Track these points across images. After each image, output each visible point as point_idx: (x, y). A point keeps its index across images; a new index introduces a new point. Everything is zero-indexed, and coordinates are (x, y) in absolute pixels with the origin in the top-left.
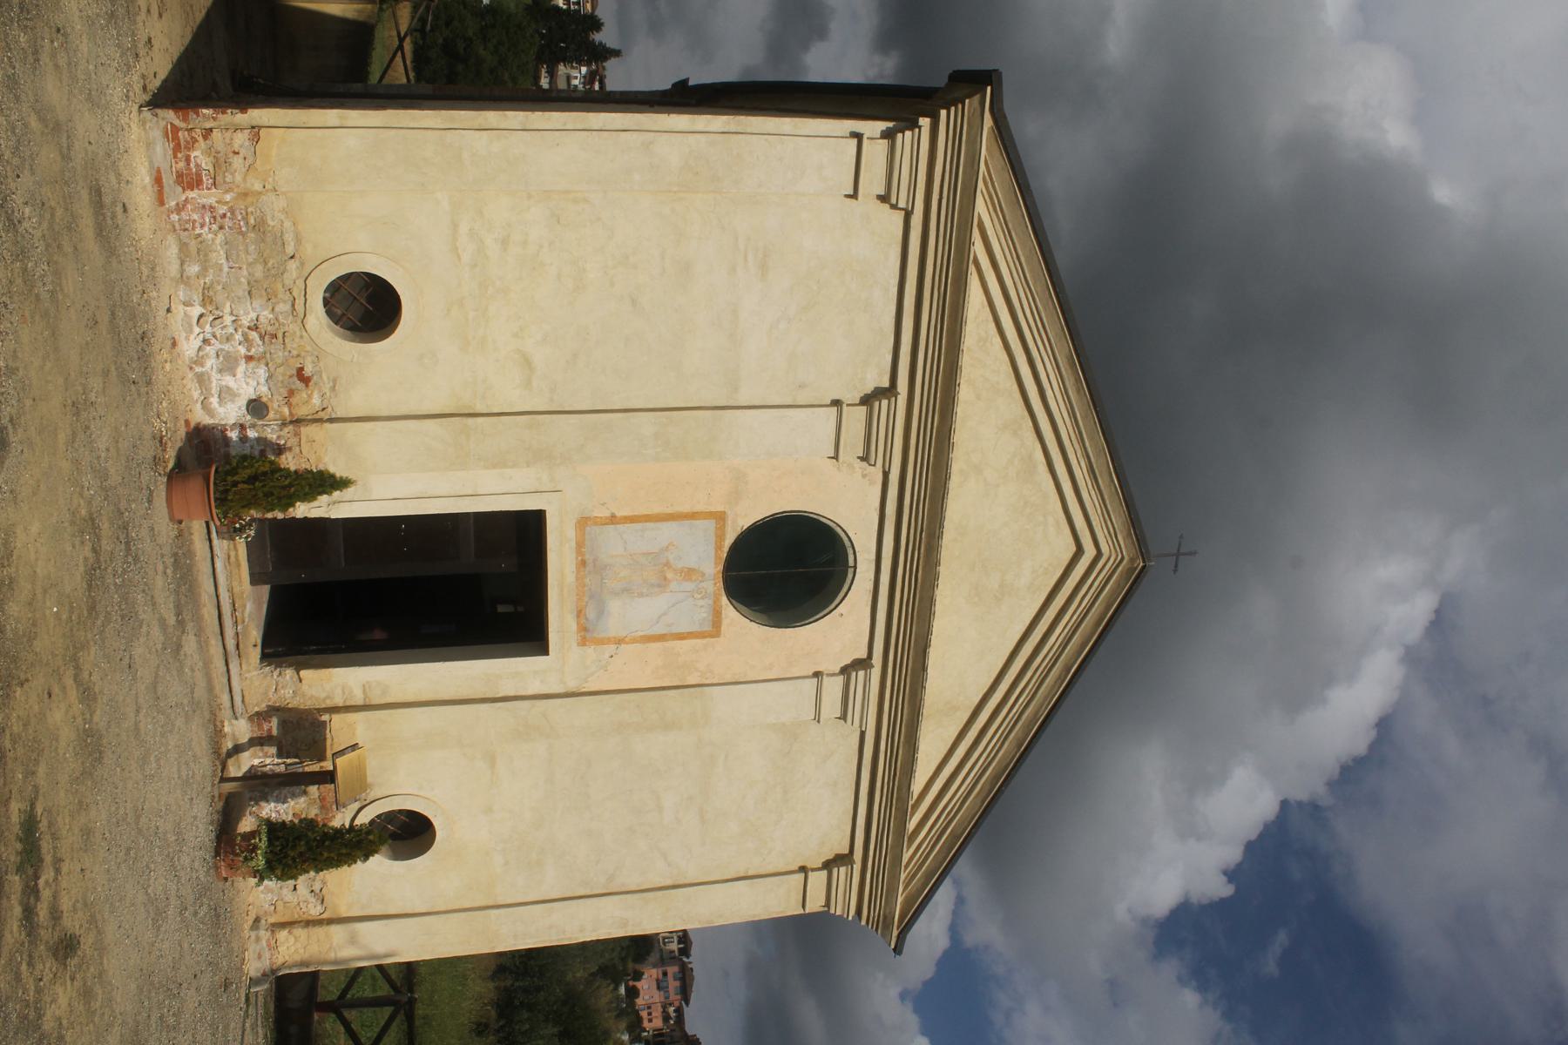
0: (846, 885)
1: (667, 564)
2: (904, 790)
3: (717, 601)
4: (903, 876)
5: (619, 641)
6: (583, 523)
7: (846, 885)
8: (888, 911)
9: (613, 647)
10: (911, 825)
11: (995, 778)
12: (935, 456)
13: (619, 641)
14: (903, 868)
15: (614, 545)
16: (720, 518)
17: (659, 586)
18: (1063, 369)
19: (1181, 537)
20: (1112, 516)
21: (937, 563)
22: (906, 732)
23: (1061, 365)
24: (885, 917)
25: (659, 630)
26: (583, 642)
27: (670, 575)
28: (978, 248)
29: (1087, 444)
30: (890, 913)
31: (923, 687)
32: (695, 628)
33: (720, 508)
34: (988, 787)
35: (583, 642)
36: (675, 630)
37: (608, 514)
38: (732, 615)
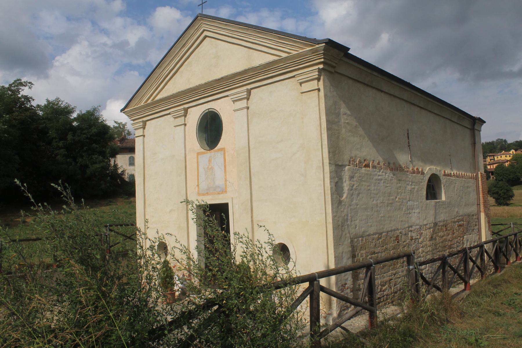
0: (304, 75)
1: (208, 168)
2: (261, 68)
3: (216, 151)
4: (301, 51)
5: (226, 180)
6: (199, 194)
7: (304, 75)
8: (309, 53)
9: (228, 182)
10: (284, 55)
11: (259, 32)
12: (178, 97)
13: (226, 180)
14: (290, 55)
15: (203, 185)
16: (198, 154)
17: (213, 169)
18: (163, 68)
19: (198, 6)
20: (192, 33)
21: (197, 86)
22: (168, 100)
23: (162, 69)
24: (313, 53)
25: (223, 168)
26: (226, 192)
27: (210, 167)
28: (149, 101)
29: (177, 52)
30: (310, 52)
31: (227, 76)
32: (223, 156)
33: (196, 154)
34: (262, 34)
35: (226, 192)
36: (223, 163)
37: (197, 187)
38: (219, 146)
